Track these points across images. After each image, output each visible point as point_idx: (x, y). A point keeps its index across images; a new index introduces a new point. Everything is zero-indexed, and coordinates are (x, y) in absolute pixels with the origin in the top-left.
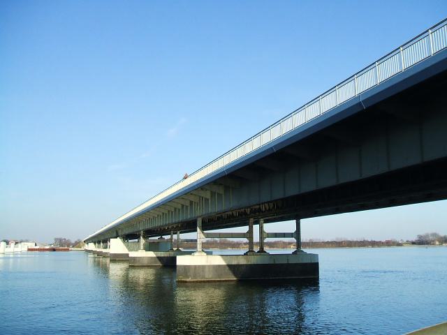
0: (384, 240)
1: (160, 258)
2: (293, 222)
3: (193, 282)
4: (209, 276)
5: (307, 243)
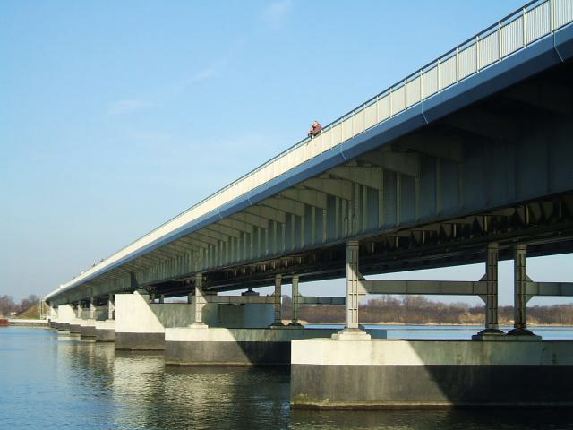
1: (246, 347)
3: (336, 409)
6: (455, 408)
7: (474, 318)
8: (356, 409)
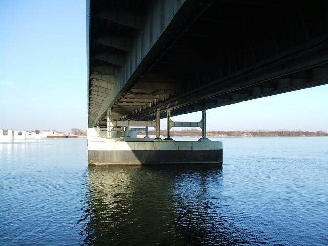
0: (315, 131)
1: (137, 153)
2: (201, 112)
3: (102, 166)
4: (116, 161)
5: (256, 132)
6: (143, 165)
7: (210, 134)
8: (109, 165)
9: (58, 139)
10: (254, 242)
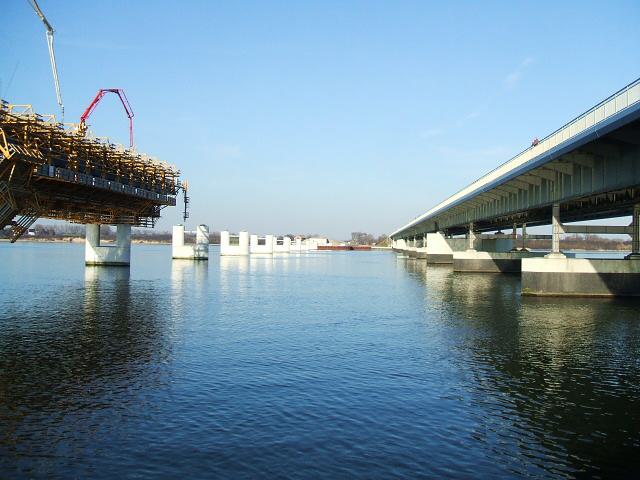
4: (569, 288)
6: (615, 297)
7: (625, 247)
8: (557, 296)
9: (336, 252)
10: (315, 468)
